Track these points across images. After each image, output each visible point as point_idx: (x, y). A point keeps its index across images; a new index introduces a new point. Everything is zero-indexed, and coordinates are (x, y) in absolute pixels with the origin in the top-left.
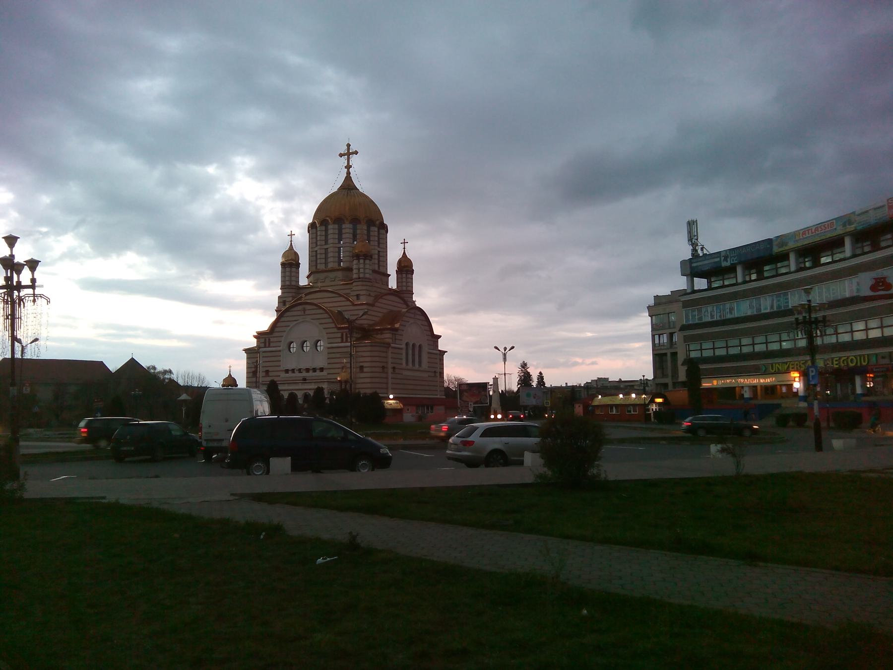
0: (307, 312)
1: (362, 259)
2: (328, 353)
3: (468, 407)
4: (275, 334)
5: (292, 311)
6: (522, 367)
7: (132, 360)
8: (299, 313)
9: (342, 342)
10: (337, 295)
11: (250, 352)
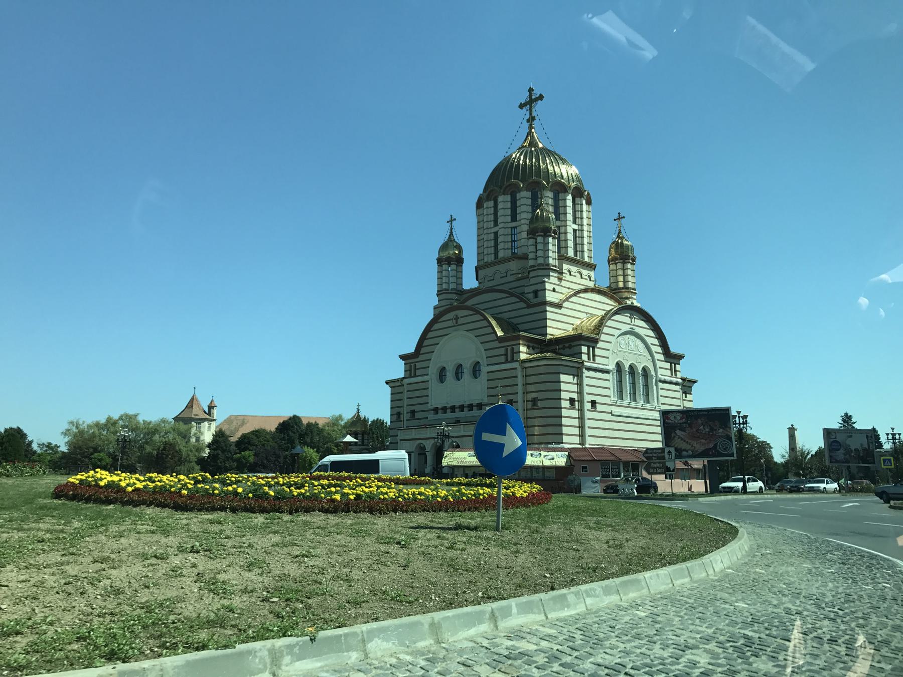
0: (460, 321)
1: (539, 236)
2: (488, 380)
3: (664, 458)
4: (421, 358)
5: (441, 322)
6: (844, 422)
7: (505, 435)
8: (450, 323)
9: (507, 362)
10: (508, 295)
11: (393, 385)
